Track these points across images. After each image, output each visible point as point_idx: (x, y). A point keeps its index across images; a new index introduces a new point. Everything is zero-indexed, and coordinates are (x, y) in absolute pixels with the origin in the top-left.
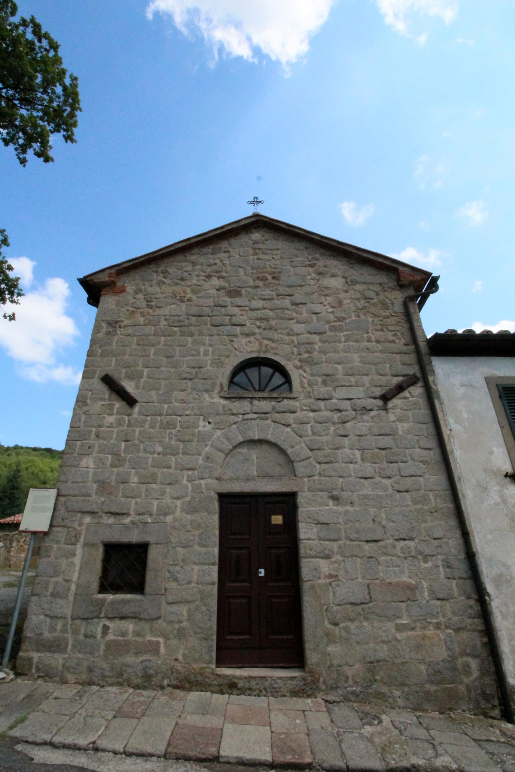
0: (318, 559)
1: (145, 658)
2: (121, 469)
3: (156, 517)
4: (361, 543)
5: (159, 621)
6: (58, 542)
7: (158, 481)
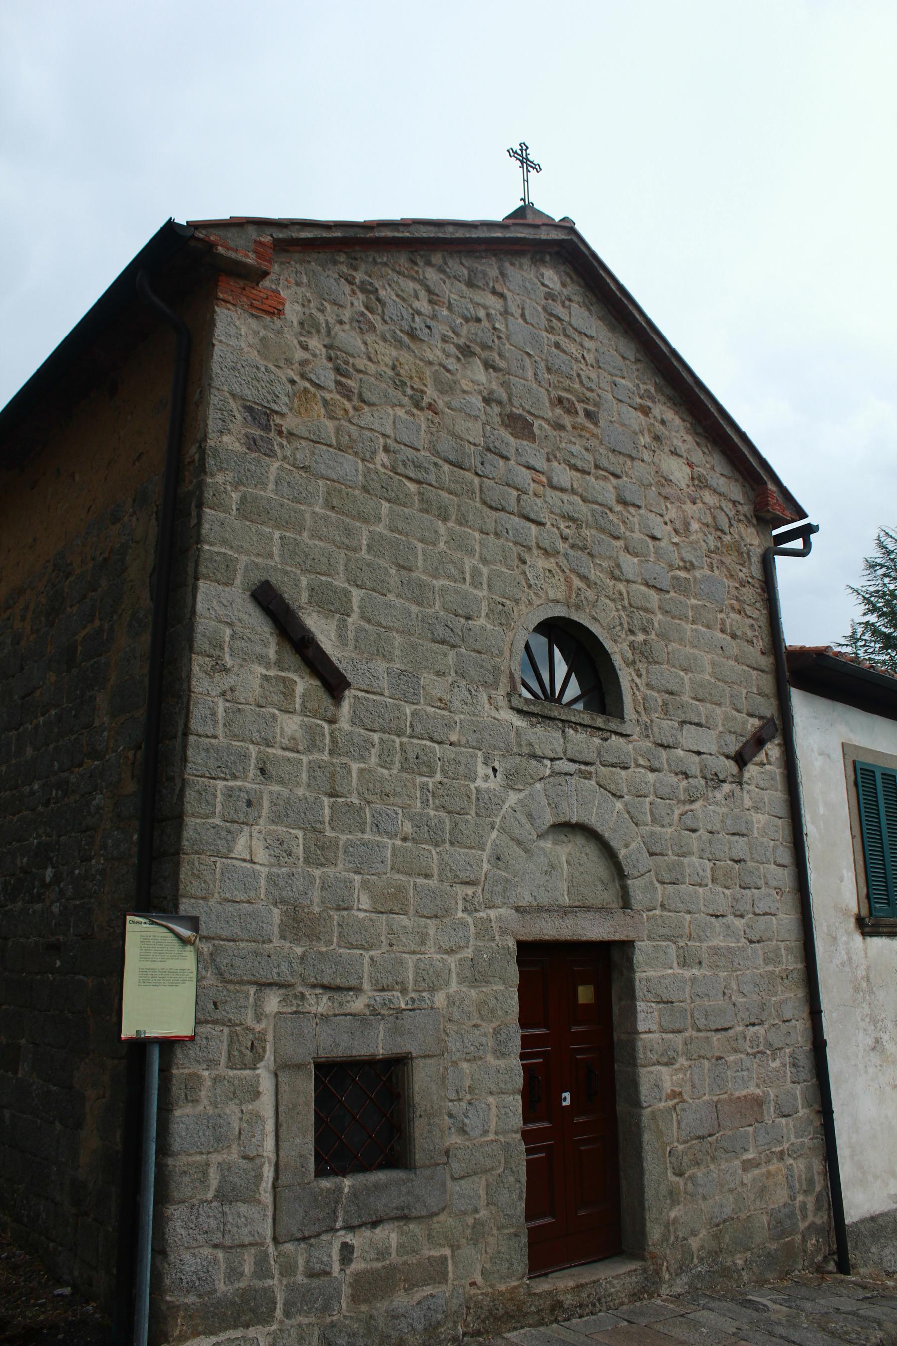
0: (659, 1068)
1: (425, 1294)
2: (330, 871)
3: (413, 995)
4: (709, 1034)
5: (442, 1218)
6: (211, 1063)
7: (411, 911)
